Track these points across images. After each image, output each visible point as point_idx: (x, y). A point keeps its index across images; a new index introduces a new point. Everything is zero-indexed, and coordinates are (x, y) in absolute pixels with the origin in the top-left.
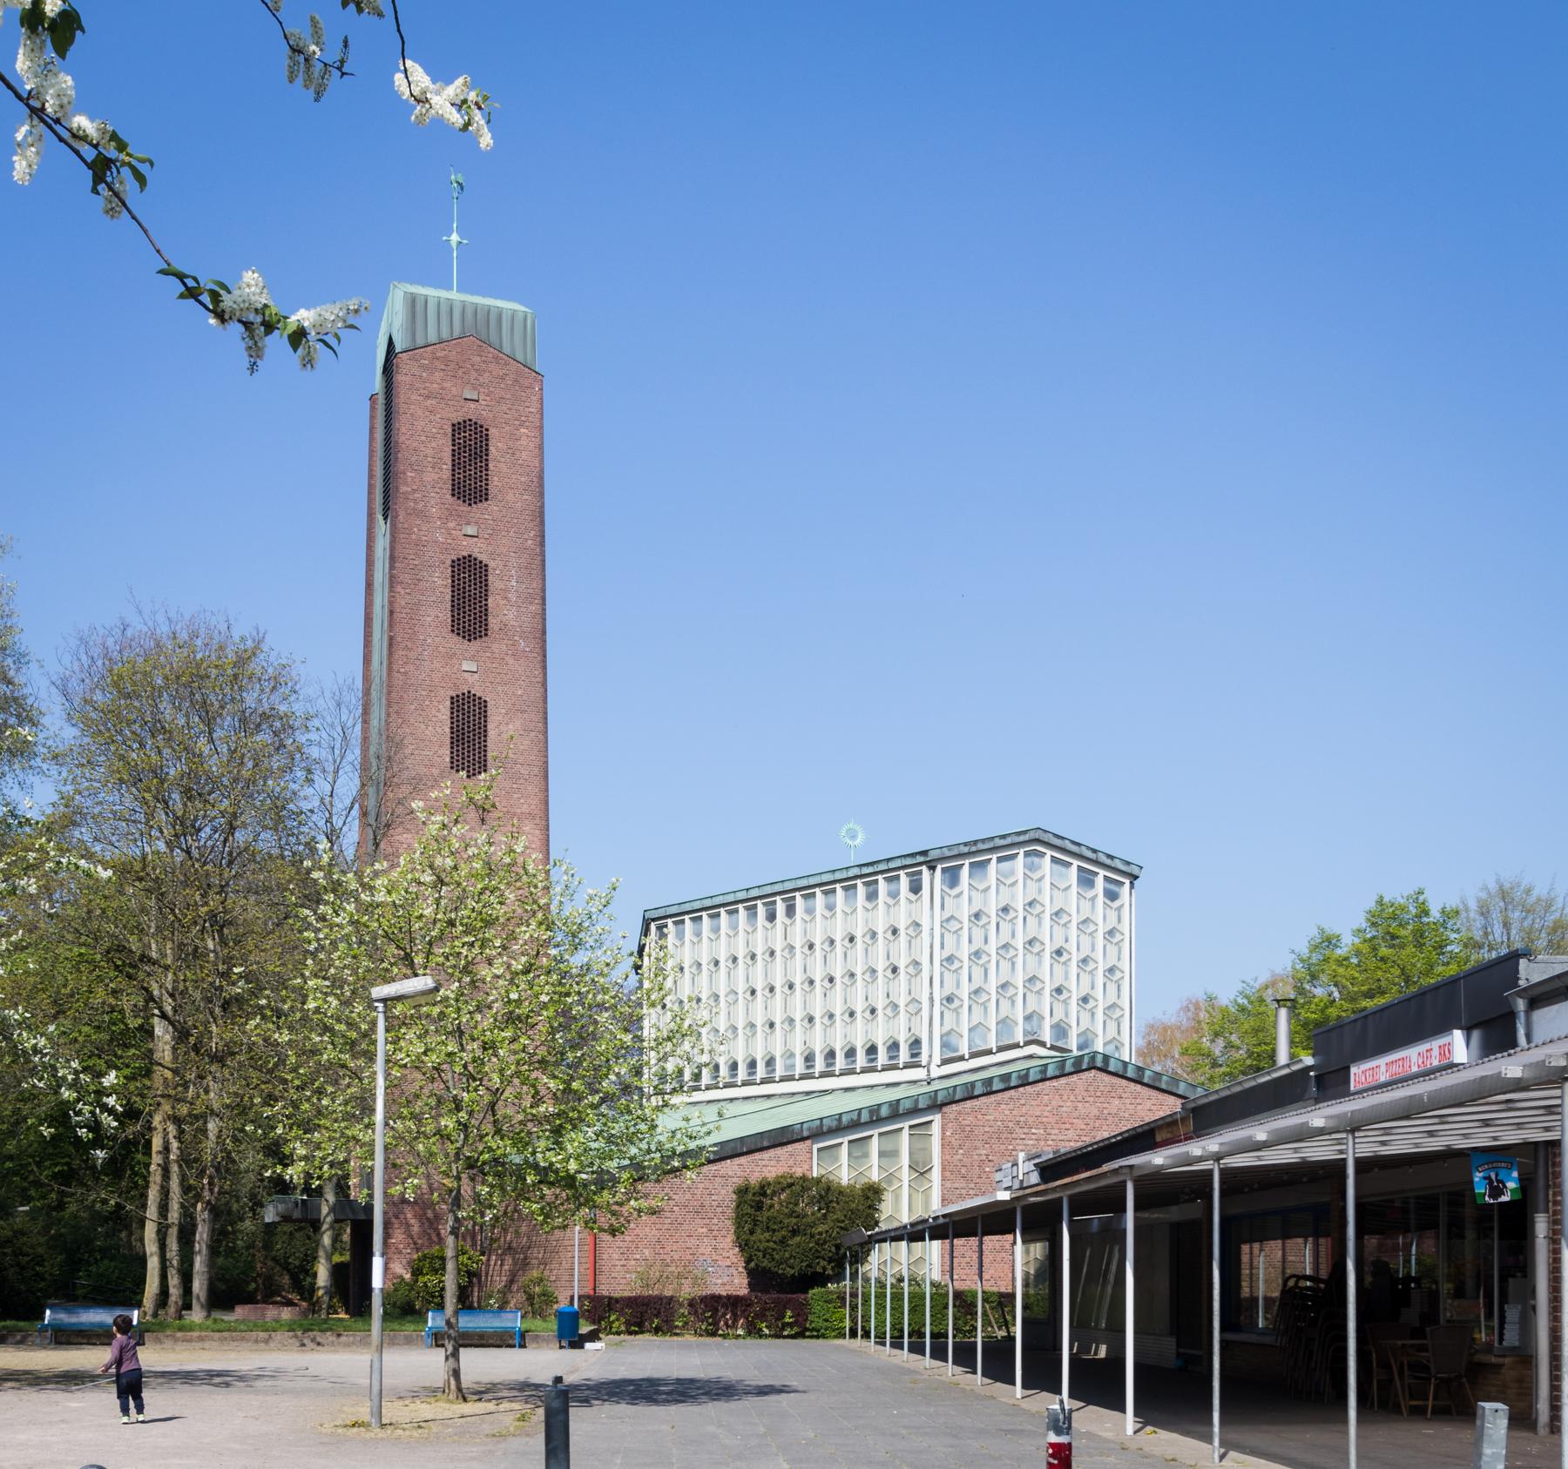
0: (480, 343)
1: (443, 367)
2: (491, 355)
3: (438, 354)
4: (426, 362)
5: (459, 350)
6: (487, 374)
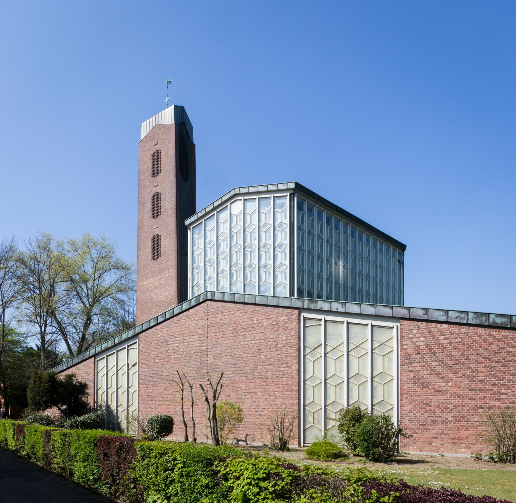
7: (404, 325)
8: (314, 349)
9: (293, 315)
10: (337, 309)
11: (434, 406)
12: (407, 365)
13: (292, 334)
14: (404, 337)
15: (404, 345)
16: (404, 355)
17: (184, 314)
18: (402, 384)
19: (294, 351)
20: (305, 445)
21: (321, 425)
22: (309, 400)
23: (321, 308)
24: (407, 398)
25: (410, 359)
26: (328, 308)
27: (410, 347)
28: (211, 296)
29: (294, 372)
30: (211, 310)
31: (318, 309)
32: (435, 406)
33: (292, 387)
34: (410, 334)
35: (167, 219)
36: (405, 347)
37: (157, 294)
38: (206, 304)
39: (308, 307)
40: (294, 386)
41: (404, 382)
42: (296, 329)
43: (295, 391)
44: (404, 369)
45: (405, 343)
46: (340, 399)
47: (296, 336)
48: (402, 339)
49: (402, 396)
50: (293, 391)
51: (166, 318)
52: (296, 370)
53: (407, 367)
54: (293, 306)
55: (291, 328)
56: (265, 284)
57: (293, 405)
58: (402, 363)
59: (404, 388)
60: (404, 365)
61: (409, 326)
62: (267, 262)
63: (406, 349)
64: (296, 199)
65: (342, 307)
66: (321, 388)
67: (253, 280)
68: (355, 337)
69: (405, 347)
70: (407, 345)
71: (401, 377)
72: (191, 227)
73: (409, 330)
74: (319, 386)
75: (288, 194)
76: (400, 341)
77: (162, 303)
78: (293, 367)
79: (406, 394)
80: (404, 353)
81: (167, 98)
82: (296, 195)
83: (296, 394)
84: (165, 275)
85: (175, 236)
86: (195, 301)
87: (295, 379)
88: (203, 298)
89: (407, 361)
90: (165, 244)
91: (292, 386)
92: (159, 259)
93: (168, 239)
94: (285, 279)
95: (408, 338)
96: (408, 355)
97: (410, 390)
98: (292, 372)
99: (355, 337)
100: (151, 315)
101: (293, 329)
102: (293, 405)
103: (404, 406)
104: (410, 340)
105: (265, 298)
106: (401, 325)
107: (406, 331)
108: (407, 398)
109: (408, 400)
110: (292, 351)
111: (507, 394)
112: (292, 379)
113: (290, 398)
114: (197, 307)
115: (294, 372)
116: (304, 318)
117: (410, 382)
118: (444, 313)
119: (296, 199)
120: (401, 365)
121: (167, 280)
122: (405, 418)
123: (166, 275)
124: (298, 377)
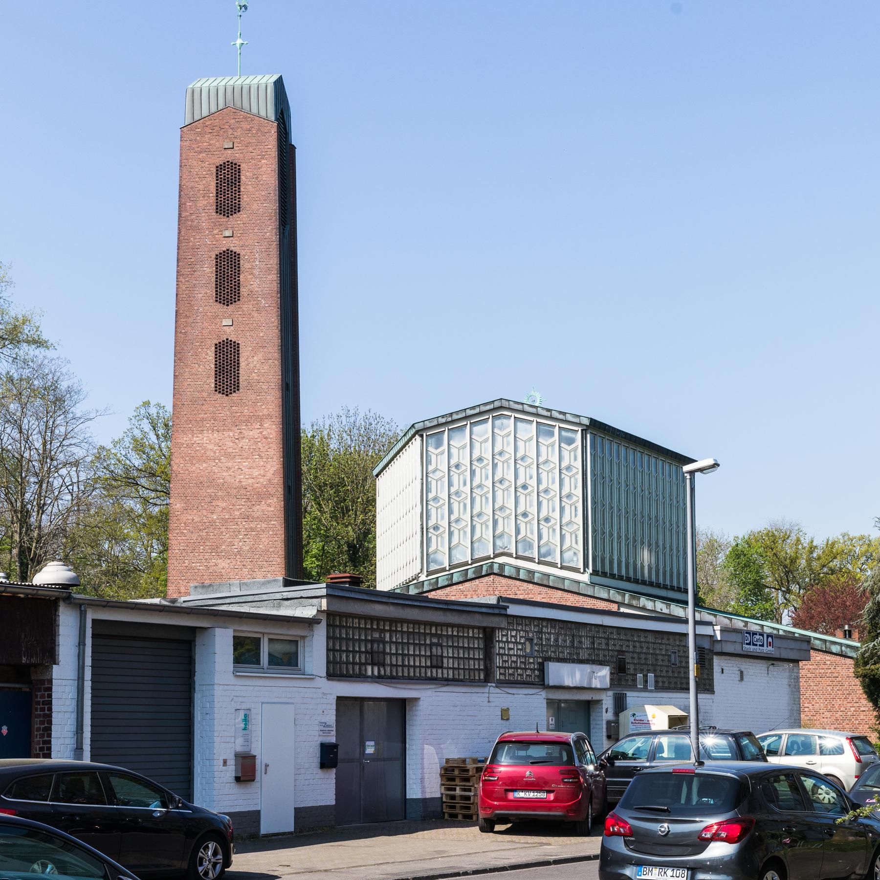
0: (233, 110)
1: (210, 131)
2: (242, 117)
3: (207, 123)
4: (199, 130)
5: (220, 118)
6: (239, 129)
10: (662, 610)
17: (455, 587)
23: (644, 606)
28: (499, 569)
30: (499, 589)
35: (255, 314)
37: (229, 468)
38: (491, 579)
51: (424, 590)
56: (547, 544)
62: (550, 514)
64: (588, 436)
65: (667, 608)
67: (529, 535)
72: (425, 434)
75: (580, 429)
77: (243, 491)
81: (239, 41)
82: (589, 431)
84: (251, 433)
85: (277, 355)
86: (474, 572)
88: (487, 571)
90: (251, 365)
92: (234, 394)
93: (260, 356)
94: (576, 543)
100: (212, 513)
105: (576, 585)
111: (808, 707)
114: (477, 580)
118: (760, 628)
119: (588, 436)
121: (257, 443)
123: (255, 433)
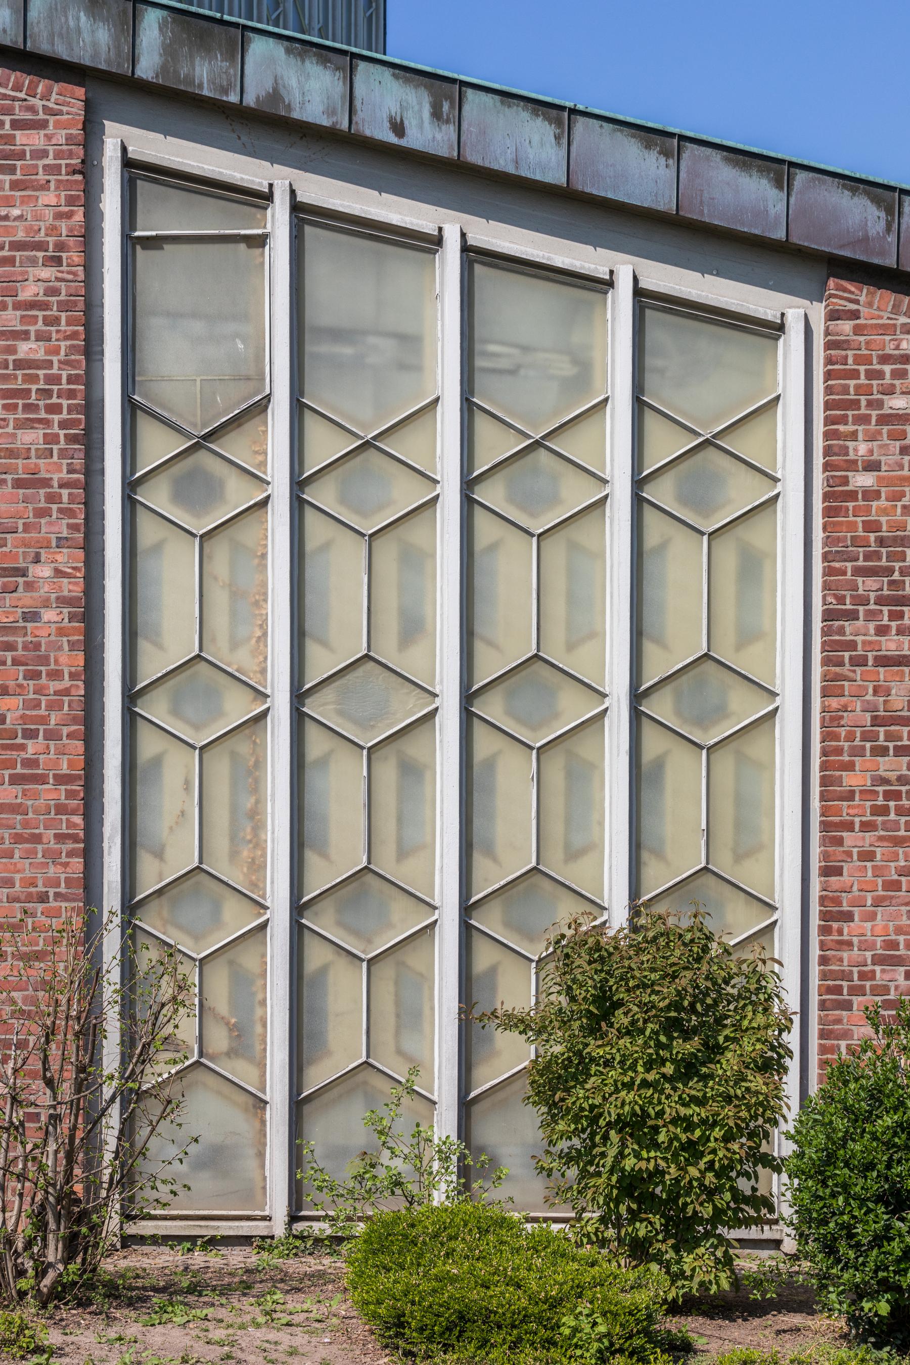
7: (855, 315)
8: (208, 437)
9: (43, 125)
10: (398, 128)
11: (865, 946)
12: (871, 615)
13: (28, 292)
14: (855, 404)
15: (852, 465)
16: (855, 541)
18: (839, 751)
19: (51, 439)
20: (132, 1229)
21: (262, 1066)
22: (159, 854)
23: (275, 96)
24: (866, 856)
25: (890, 571)
26: (330, 111)
27: (890, 481)
29: (49, 615)
31: (250, 100)
32: (871, 947)
33: (32, 747)
34: (890, 391)
36: (862, 480)
39: (164, 69)
40: (52, 735)
41: (850, 737)
42: (61, 247)
43: (61, 779)
44: (852, 646)
45: (861, 448)
46: (402, 854)
47: (64, 306)
48: (843, 420)
49: (840, 842)
50: (41, 779)
52: (63, 601)
53: (872, 626)
54: (42, 44)
55: (21, 236)
57: (43, 898)
58: (841, 600)
59: (851, 780)
60: (852, 616)
61: (887, 329)
63: (871, 495)
65: (436, 114)
66: (259, 764)
68: (513, 372)
69: (862, 480)
70: (872, 466)
71: (834, 703)
73: (885, 359)
74: (242, 746)
76: (827, 435)
78: (44, 571)
79: (867, 827)
80: (852, 526)
83: (61, 809)
87: (56, 675)
89: (871, 583)
91: (31, 734)
95: (884, 420)
96: (881, 542)
97: (888, 795)
98: (32, 616)
99: (513, 372)
101: (40, 246)
102: (43, 898)
103: (848, 917)
104: (892, 437)
106: (833, 316)
107: (867, 360)
108: (866, 856)
109: (878, 872)
110: (31, 438)
112: (36, 675)
113: (18, 839)
115: (49, 615)
116: (128, 163)
117: (889, 737)
120: (829, 616)
122: (856, 1000)
124: (80, 658)
